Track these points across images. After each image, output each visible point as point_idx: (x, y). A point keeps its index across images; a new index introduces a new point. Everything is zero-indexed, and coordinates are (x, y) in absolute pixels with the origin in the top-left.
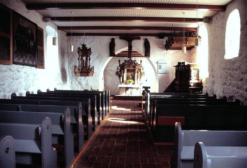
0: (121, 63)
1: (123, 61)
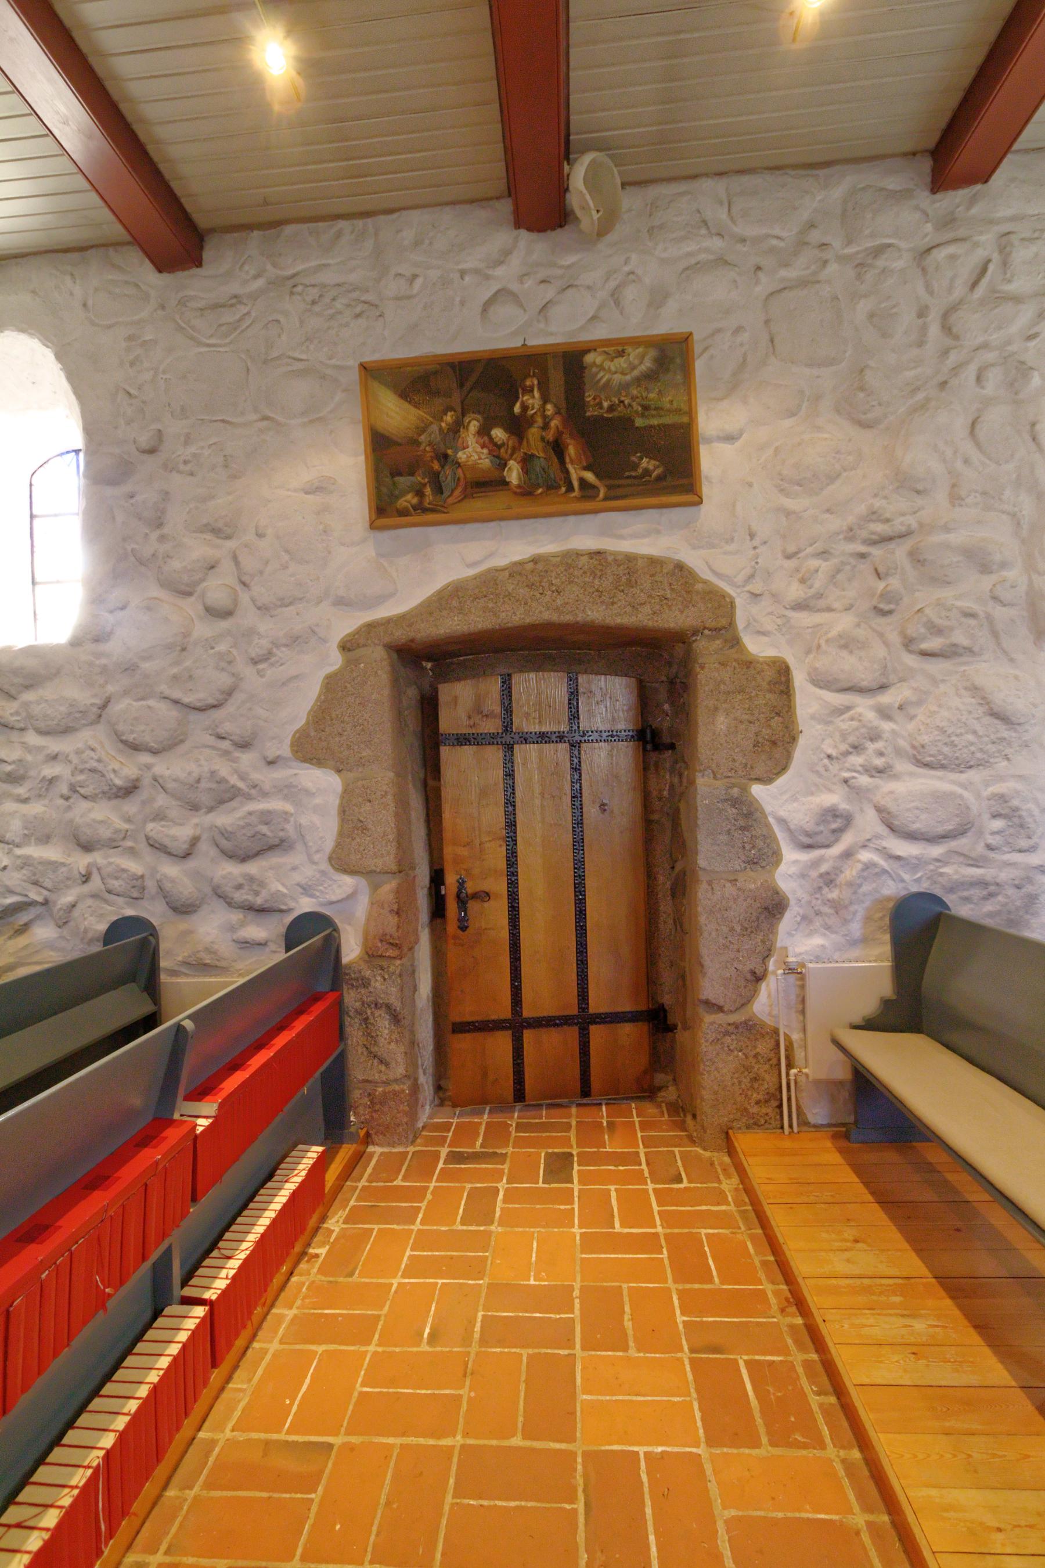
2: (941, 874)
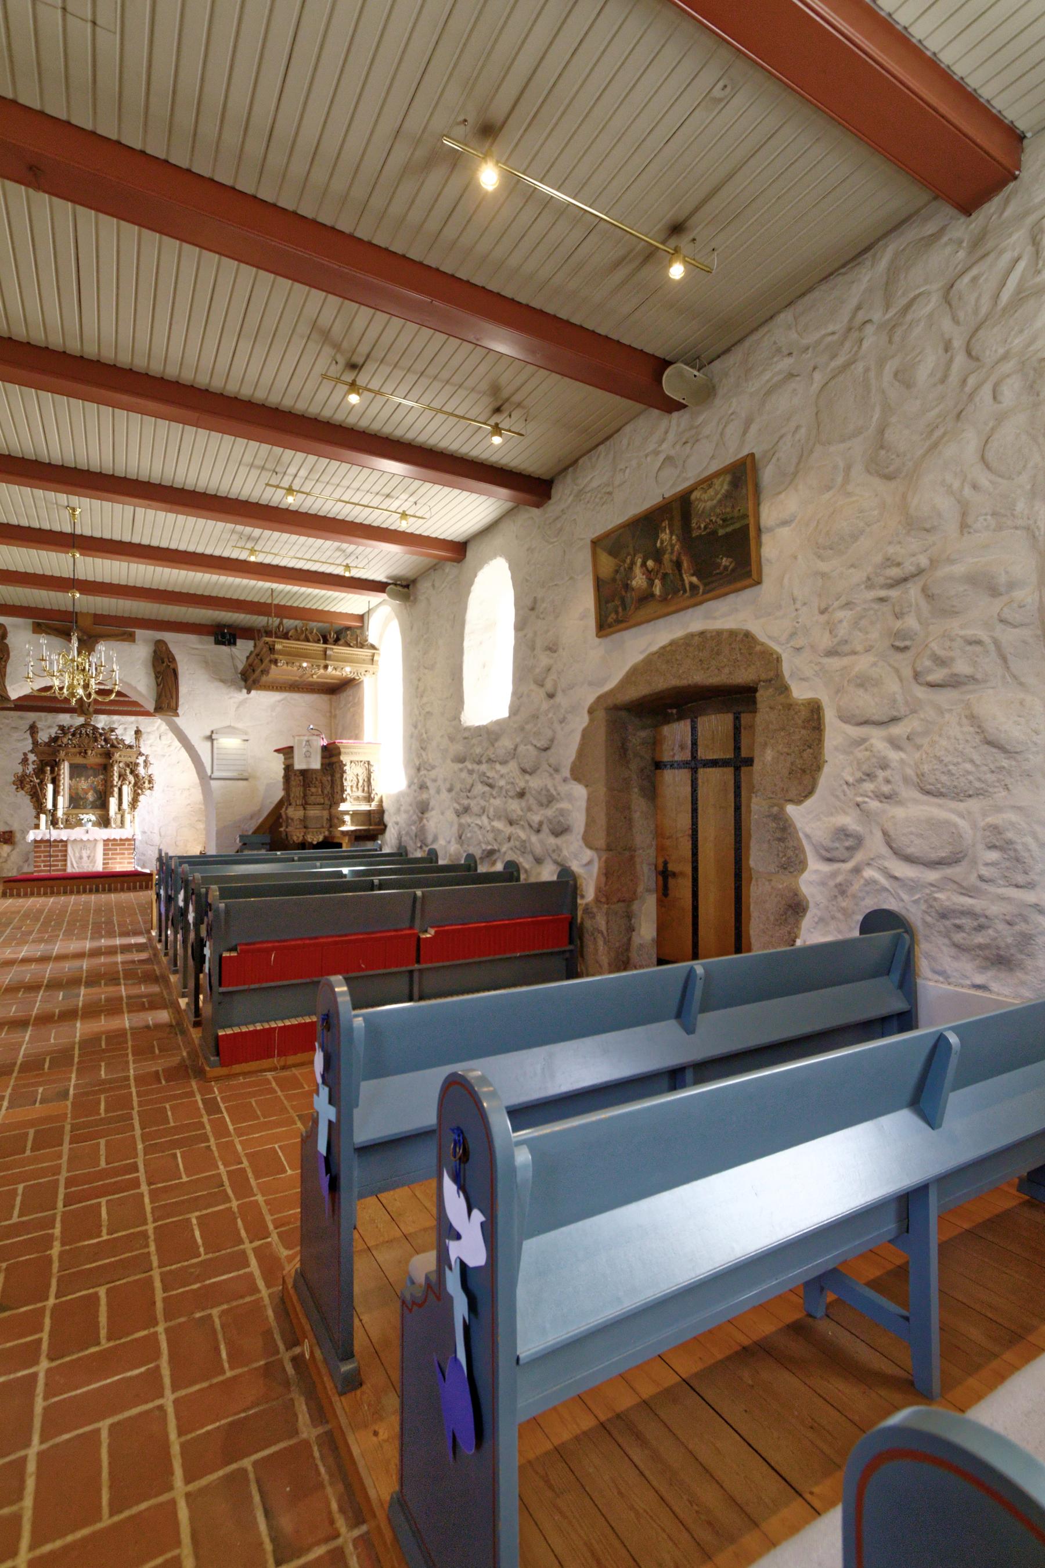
0: (43, 737)
1: (54, 731)
2: (935, 899)
